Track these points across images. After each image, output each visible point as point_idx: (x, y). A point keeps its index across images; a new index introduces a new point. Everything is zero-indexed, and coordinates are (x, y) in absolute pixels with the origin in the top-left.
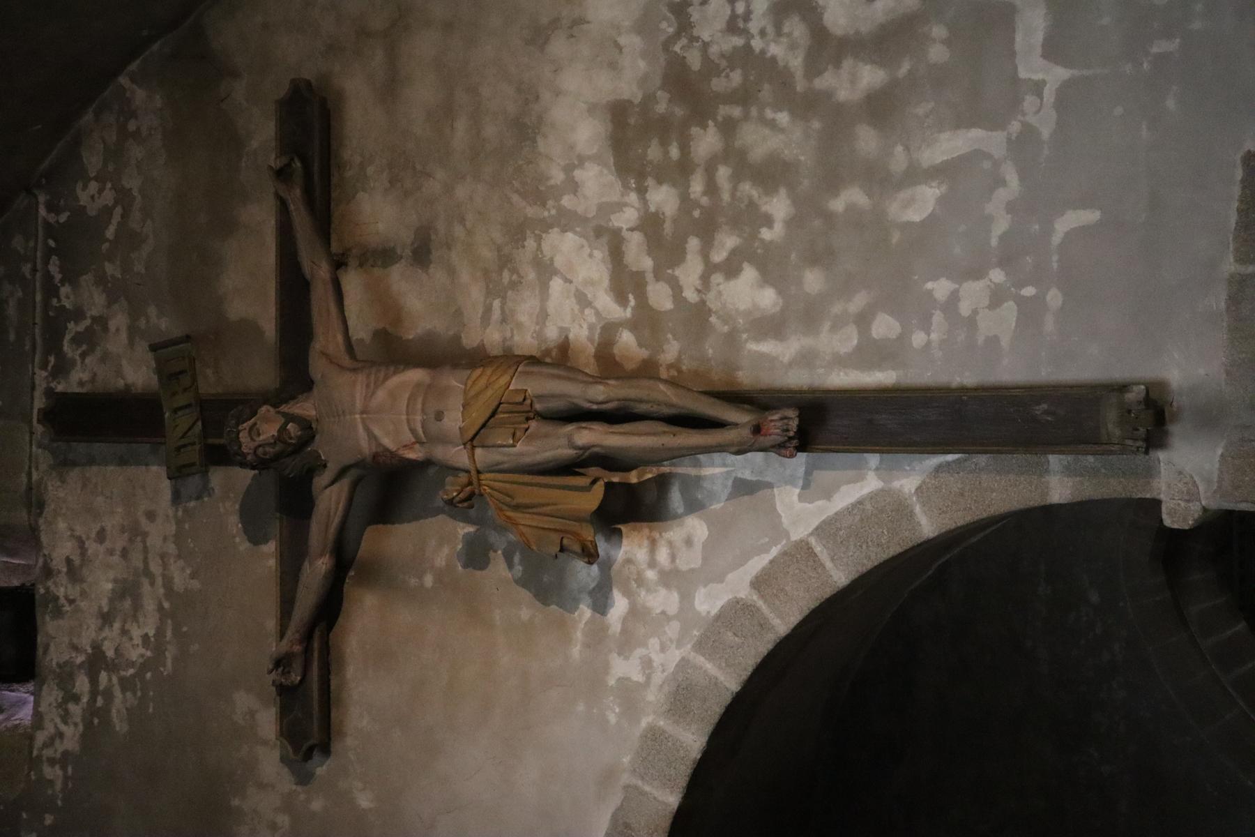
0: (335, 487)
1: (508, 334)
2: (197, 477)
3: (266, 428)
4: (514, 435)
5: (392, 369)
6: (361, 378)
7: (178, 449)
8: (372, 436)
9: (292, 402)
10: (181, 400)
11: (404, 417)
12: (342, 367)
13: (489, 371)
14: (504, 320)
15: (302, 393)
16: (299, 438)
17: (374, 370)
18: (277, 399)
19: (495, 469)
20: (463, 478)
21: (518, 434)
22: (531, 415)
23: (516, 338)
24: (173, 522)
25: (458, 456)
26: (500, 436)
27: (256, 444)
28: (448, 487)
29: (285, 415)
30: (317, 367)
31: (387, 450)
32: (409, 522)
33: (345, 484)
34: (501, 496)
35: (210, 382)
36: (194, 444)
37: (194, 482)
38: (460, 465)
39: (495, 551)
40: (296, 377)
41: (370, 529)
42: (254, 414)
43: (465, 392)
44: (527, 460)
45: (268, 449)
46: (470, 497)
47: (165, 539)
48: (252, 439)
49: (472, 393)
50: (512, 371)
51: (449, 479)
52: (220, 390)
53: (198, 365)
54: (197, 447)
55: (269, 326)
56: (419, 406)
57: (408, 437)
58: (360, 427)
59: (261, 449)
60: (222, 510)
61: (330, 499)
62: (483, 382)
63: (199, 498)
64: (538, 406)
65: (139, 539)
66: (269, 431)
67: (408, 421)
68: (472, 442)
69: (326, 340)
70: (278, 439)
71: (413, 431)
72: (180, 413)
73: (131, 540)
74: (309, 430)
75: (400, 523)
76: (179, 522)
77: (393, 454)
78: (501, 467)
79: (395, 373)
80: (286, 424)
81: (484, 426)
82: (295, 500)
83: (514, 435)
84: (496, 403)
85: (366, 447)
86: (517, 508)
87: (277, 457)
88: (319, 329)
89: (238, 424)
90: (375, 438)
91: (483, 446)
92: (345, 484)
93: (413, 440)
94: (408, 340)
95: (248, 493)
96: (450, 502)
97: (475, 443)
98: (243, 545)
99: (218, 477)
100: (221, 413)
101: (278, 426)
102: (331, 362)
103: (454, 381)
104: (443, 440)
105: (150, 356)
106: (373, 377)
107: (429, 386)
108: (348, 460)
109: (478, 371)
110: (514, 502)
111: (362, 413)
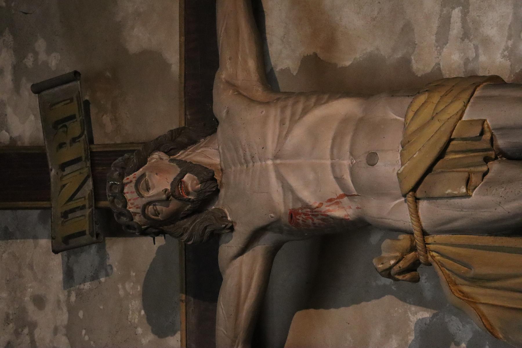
0: (246, 257)
1: (471, 54)
4: (468, 181)
5: (313, 100)
6: (274, 114)
7: (65, 215)
8: (287, 188)
9: (191, 148)
10: (69, 153)
11: (329, 162)
13: (436, 98)
14: (466, 35)
15: (205, 137)
16: (198, 192)
17: (290, 102)
18: (173, 143)
19: (447, 228)
20: (404, 241)
21: (474, 179)
22: (492, 154)
23: (483, 58)
24: (65, 309)
25: (397, 212)
26: (450, 183)
27: (144, 201)
28: (384, 254)
29: (180, 163)
30: (223, 101)
31: (307, 206)
32: (347, 305)
33: (259, 250)
34: (456, 266)
35: (106, 132)
36: (83, 207)
37: (88, 258)
38: (400, 225)
39: (458, 344)
40: (201, 119)
41: (298, 315)
42: (143, 162)
43: (405, 126)
44: (485, 215)
45: (159, 207)
46: (414, 266)
47: (56, 331)
49: (413, 127)
50: (465, 96)
51: (387, 242)
53: (93, 111)
54: (87, 212)
55: (173, 57)
56: (347, 147)
57: (334, 189)
58: (273, 176)
60: (121, 292)
61: (241, 273)
62: (427, 113)
63: (95, 277)
64: (501, 142)
65: (26, 331)
66: (160, 184)
67: (333, 166)
68: (415, 192)
69: (237, 65)
71: (339, 180)
72: (68, 170)
73: (17, 333)
74: (212, 184)
75: (337, 307)
76: (72, 311)
77: (314, 212)
78: (456, 224)
79: (318, 104)
80: (182, 175)
81: (429, 170)
82: (202, 276)
83: (468, 181)
84: (444, 139)
85: (281, 204)
86: (477, 280)
87: (173, 218)
88: (225, 54)
89: (122, 176)
90: (292, 191)
91: (429, 198)
92: (259, 250)
93: (341, 192)
94: (344, 68)
95: (151, 272)
96: (387, 273)
97: (418, 194)
98: (147, 337)
99: (116, 249)
100: (107, 164)
103: (390, 112)
104: (377, 191)
105: (34, 100)
106: (288, 112)
107: (361, 120)
108: (260, 223)
109: (422, 98)
110: (472, 273)
111: (276, 157)
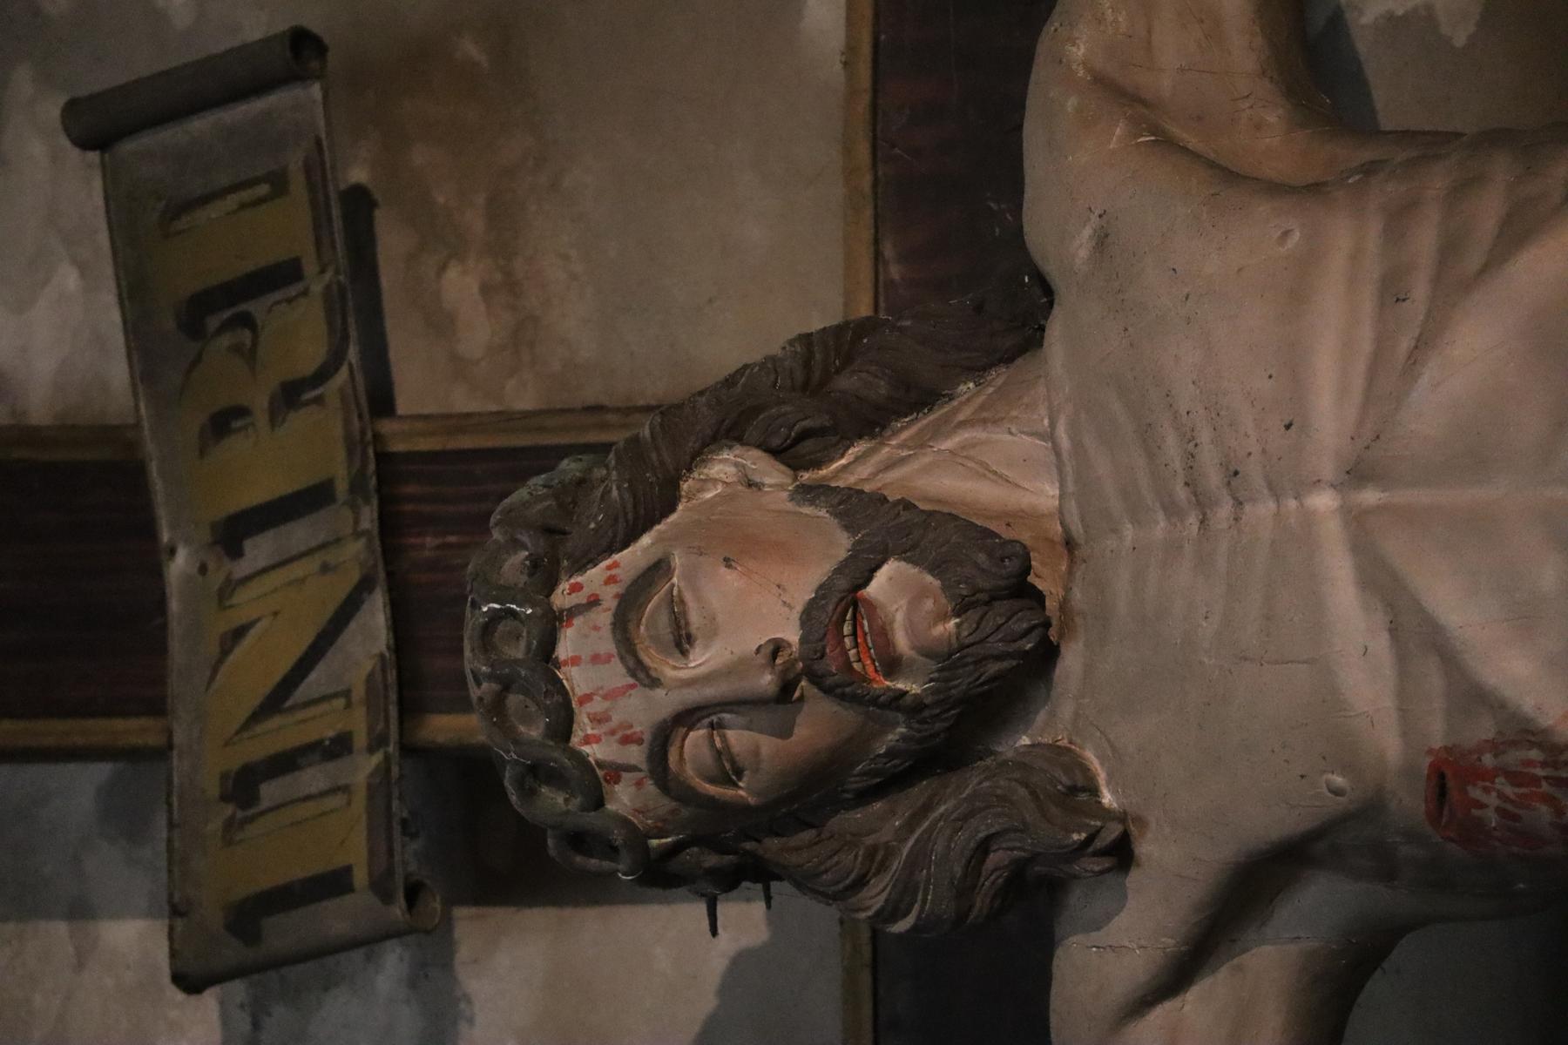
0: (1198, 1005)
2: (393, 962)
3: (743, 584)
7: (243, 786)
8: (1415, 635)
9: (907, 431)
10: (263, 465)
12: (1229, 177)
15: (977, 370)
16: (948, 659)
17: (1438, 180)
18: (812, 404)
27: (666, 702)
29: (852, 506)
30: (1078, 186)
31: (1527, 733)
35: (455, 358)
36: (340, 746)
45: (738, 738)
48: (643, 675)
52: (523, 397)
53: (392, 242)
54: (363, 767)
59: (696, 739)
66: (747, 613)
70: (794, 679)
72: (259, 550)
74: (1013, 611)
80: (860, 569)
85: (1379, 715)
87: (813, 793)
89: (545, 574)
101: (804, 583)
102: (1166, 143)
111: (1357, 474)
